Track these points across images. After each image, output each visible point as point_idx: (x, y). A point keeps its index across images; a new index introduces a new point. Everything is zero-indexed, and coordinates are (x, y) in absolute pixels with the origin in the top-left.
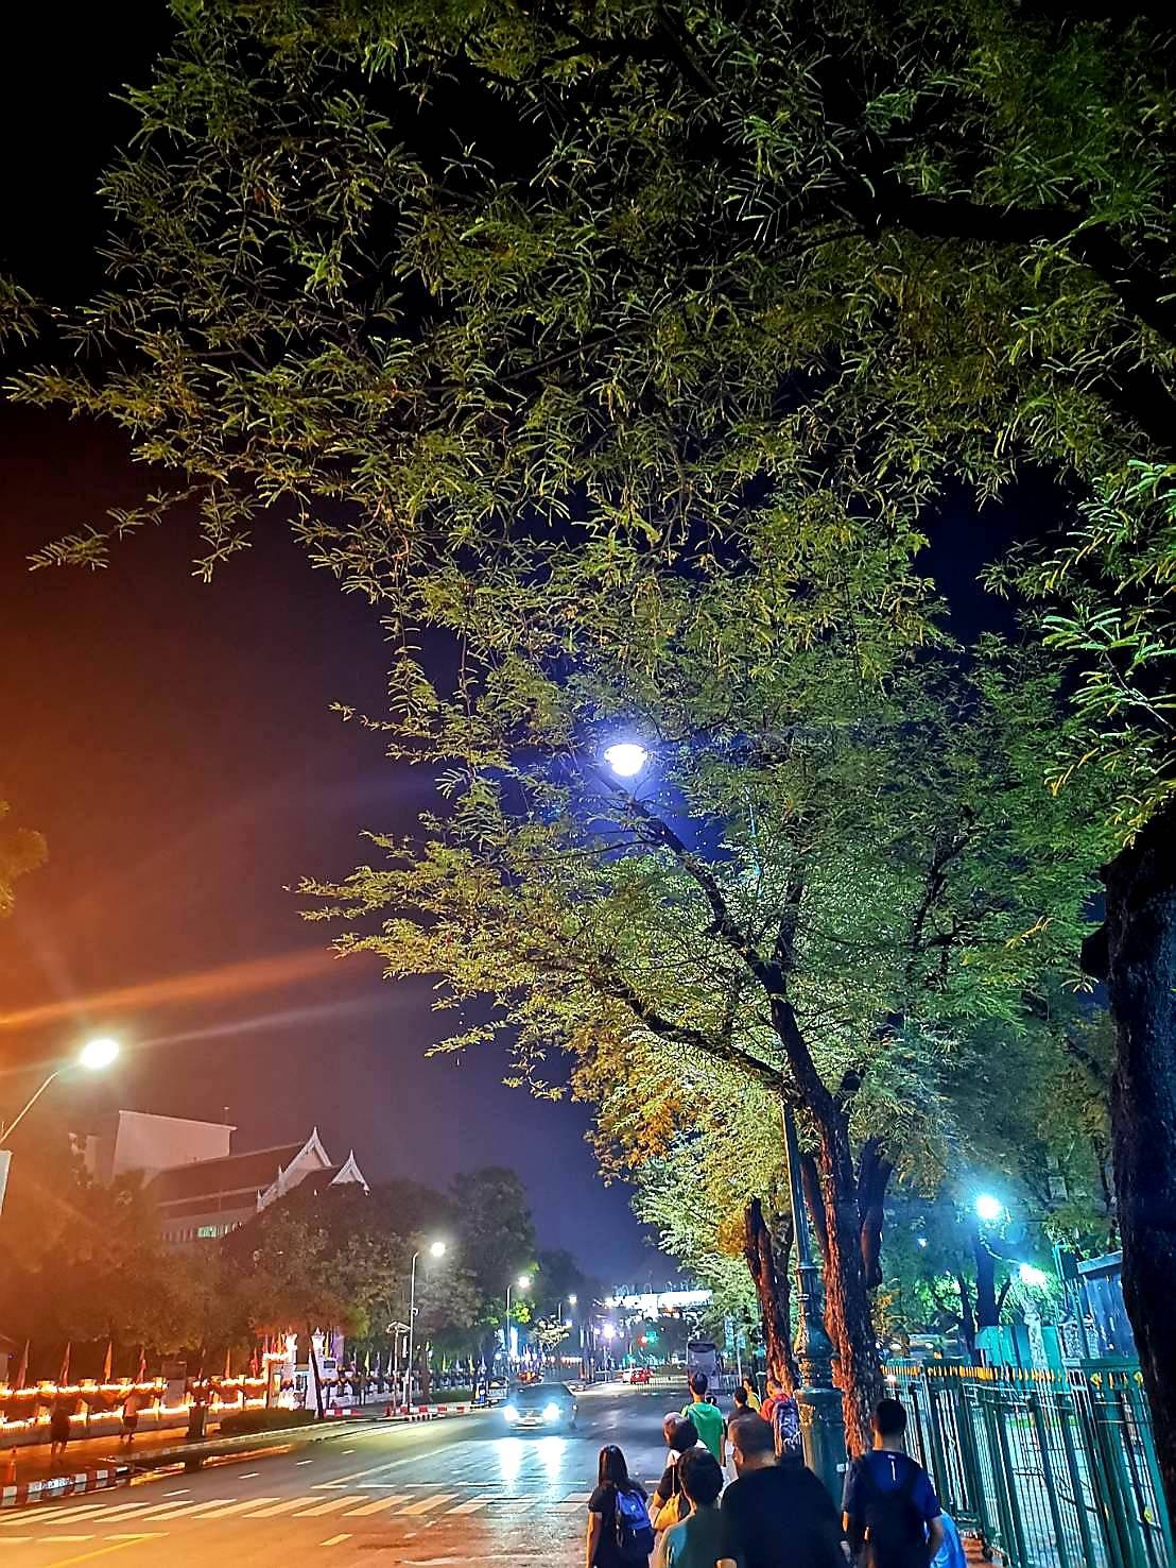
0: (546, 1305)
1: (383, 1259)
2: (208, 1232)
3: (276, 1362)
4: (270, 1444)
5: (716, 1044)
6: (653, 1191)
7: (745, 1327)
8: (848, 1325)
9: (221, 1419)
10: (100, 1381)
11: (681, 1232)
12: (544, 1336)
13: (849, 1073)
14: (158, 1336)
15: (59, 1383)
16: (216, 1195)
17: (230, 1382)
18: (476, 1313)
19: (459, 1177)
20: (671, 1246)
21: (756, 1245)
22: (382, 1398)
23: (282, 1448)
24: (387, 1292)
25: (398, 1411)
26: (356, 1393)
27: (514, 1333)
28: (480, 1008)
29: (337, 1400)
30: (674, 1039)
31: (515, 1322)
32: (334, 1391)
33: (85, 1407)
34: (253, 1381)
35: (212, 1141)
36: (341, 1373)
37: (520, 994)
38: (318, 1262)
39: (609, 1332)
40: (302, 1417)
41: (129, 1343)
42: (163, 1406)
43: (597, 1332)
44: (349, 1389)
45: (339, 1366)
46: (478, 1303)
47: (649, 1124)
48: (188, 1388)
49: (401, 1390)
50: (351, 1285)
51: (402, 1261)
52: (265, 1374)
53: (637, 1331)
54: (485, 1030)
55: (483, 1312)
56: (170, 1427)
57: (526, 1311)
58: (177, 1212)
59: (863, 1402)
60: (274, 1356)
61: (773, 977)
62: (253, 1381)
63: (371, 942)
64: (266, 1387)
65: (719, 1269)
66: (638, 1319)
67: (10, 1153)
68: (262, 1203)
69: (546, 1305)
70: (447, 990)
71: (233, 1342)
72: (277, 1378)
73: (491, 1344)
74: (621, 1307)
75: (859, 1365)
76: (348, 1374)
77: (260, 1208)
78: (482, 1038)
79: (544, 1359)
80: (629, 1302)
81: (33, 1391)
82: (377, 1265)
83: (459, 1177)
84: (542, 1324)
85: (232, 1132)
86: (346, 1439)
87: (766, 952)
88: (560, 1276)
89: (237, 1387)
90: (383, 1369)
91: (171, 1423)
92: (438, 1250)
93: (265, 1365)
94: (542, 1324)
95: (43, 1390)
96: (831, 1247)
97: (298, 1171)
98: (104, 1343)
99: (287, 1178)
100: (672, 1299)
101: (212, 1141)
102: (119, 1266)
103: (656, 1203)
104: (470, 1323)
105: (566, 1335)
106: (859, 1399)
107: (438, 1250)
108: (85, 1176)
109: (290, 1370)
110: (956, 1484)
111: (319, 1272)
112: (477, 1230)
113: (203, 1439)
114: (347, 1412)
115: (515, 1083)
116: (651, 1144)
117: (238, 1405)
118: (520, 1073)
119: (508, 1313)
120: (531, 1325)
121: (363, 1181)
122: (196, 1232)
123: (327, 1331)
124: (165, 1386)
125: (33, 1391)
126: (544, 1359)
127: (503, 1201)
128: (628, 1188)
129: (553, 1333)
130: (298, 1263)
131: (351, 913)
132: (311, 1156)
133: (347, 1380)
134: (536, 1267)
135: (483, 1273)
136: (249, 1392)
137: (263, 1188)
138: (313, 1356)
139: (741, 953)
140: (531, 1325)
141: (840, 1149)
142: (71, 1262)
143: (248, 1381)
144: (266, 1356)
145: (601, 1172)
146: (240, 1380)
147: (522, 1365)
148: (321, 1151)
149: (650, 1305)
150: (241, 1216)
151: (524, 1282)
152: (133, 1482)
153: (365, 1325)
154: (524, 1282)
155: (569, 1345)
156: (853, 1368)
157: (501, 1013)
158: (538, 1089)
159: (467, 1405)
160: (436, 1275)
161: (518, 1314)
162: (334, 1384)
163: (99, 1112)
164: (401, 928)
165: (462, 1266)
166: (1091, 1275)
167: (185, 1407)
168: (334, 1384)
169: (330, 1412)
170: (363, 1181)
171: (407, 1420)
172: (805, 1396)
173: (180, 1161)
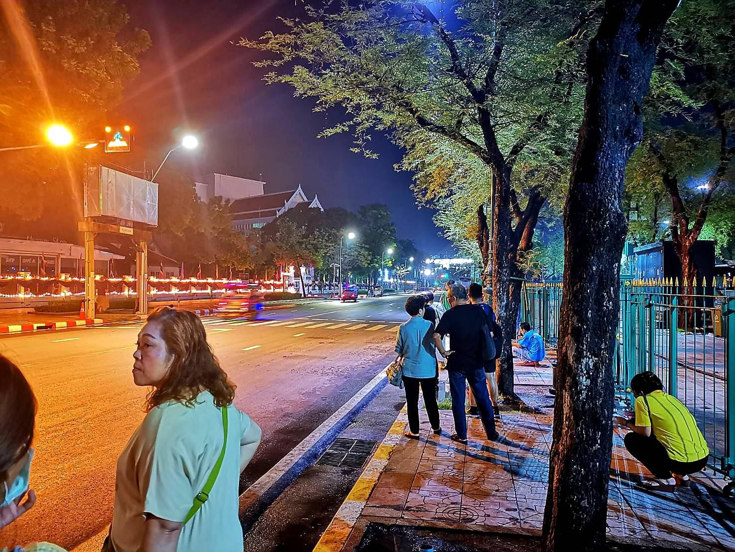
0: (399, 260)
1: (329, 239)
4: (283, 304)
5: (453, 133)
7: (479, 269)
8: (497, 258)
11: (455, 231)
12: (399, 272)
13: (515, 147)
14: (236, 263)
16: (258, 211)
17: (268, 282)
18: (369, 262)
19: (362, 207)
20: (449, 236)
21: (482, 234)
22: (330, 291)
24: (331, 252)
26: (320, 289)
27: (387, 272)
28: (338, 112)
29: (312, 291)
30: (431, 130)
31: (386, 267)
32: (311, 288)
34: (277, 283)
35: (255, 188)
36: (314, 282)
38: (303, 238)
39: (427, 272)
40: (297, 296)
43: (422, 272)
44: (317, 288)
45: (313, 279)
46: (370, 258)
50: (316, 249)
51: (336, 239)
52: (282, 280)
53: (439, 273)
54: (344, 126)
55: (372, 262)
57: (390, 262)
59: (499, 288)
61: (479, 96)
62: (277, 283)
64: (282, 285)
65: (469, 246)
66: (441, 268)
68: (278, 214)
69: (399, 260)
71: (267, 266)
72: (287, 282)
73: (376, 275)
74: (433, 263)
75: (500, 274)
76: (316, 282)
79: (399, 281)
80: (437, 262)
82: (326, 241)
83: (362, 207)
84: (398, 268)
86: (314, 304)
87: (478, 84)
88: (406, 249)
92: (352, 236)
93: (282, 277)
94: (398, 268)
96: (494, 226)
99: (288, 205)
100: (455, 261)
101: (255, 188)
102: (216, 235)
104: (366, 265)
106: (498, 287)
107: (352, 236)
109: (291, 278)
111: (302, 243)
112: (370, 229)
114: (315, 296)
115: (356, 150)
117: (272, 291)
118: (358, 146)
119: (383, 263)
120: (393, 268)
122: (252, 225)
123: (307, 265)
125: (188, 281)
126: (399, 281)
127: (381, 218)
128: (430, 211)
129: (402, 272)
130: (294, 239)
131: (277, 63)
132: (298, 197)
135: (372, 244)
137: (279, 208)
139: (464, 83)
141: (505, 182)
142: (196, 233)
143: (275, 282)
144: (282, 274)
145: (416, 203)
146: (272, 282)
147: (390, 284)
148: (303, 194)
149: (446, 263)
150: (270, 219)
151: (390, 251)
153: (321, 264)
154: (390, 251)
155: (410, 276)
156: (497, 275)
157: (350, 117)
158: (367, 154)
159: (365, 296)
162: (311, 285)
164: (299, 70)
165: (363, 243)
166: (639, 253)
168: (311, 285)
169: (310, 295)
171: (339, 299)
172: (487, 290)
173: (242, 197)
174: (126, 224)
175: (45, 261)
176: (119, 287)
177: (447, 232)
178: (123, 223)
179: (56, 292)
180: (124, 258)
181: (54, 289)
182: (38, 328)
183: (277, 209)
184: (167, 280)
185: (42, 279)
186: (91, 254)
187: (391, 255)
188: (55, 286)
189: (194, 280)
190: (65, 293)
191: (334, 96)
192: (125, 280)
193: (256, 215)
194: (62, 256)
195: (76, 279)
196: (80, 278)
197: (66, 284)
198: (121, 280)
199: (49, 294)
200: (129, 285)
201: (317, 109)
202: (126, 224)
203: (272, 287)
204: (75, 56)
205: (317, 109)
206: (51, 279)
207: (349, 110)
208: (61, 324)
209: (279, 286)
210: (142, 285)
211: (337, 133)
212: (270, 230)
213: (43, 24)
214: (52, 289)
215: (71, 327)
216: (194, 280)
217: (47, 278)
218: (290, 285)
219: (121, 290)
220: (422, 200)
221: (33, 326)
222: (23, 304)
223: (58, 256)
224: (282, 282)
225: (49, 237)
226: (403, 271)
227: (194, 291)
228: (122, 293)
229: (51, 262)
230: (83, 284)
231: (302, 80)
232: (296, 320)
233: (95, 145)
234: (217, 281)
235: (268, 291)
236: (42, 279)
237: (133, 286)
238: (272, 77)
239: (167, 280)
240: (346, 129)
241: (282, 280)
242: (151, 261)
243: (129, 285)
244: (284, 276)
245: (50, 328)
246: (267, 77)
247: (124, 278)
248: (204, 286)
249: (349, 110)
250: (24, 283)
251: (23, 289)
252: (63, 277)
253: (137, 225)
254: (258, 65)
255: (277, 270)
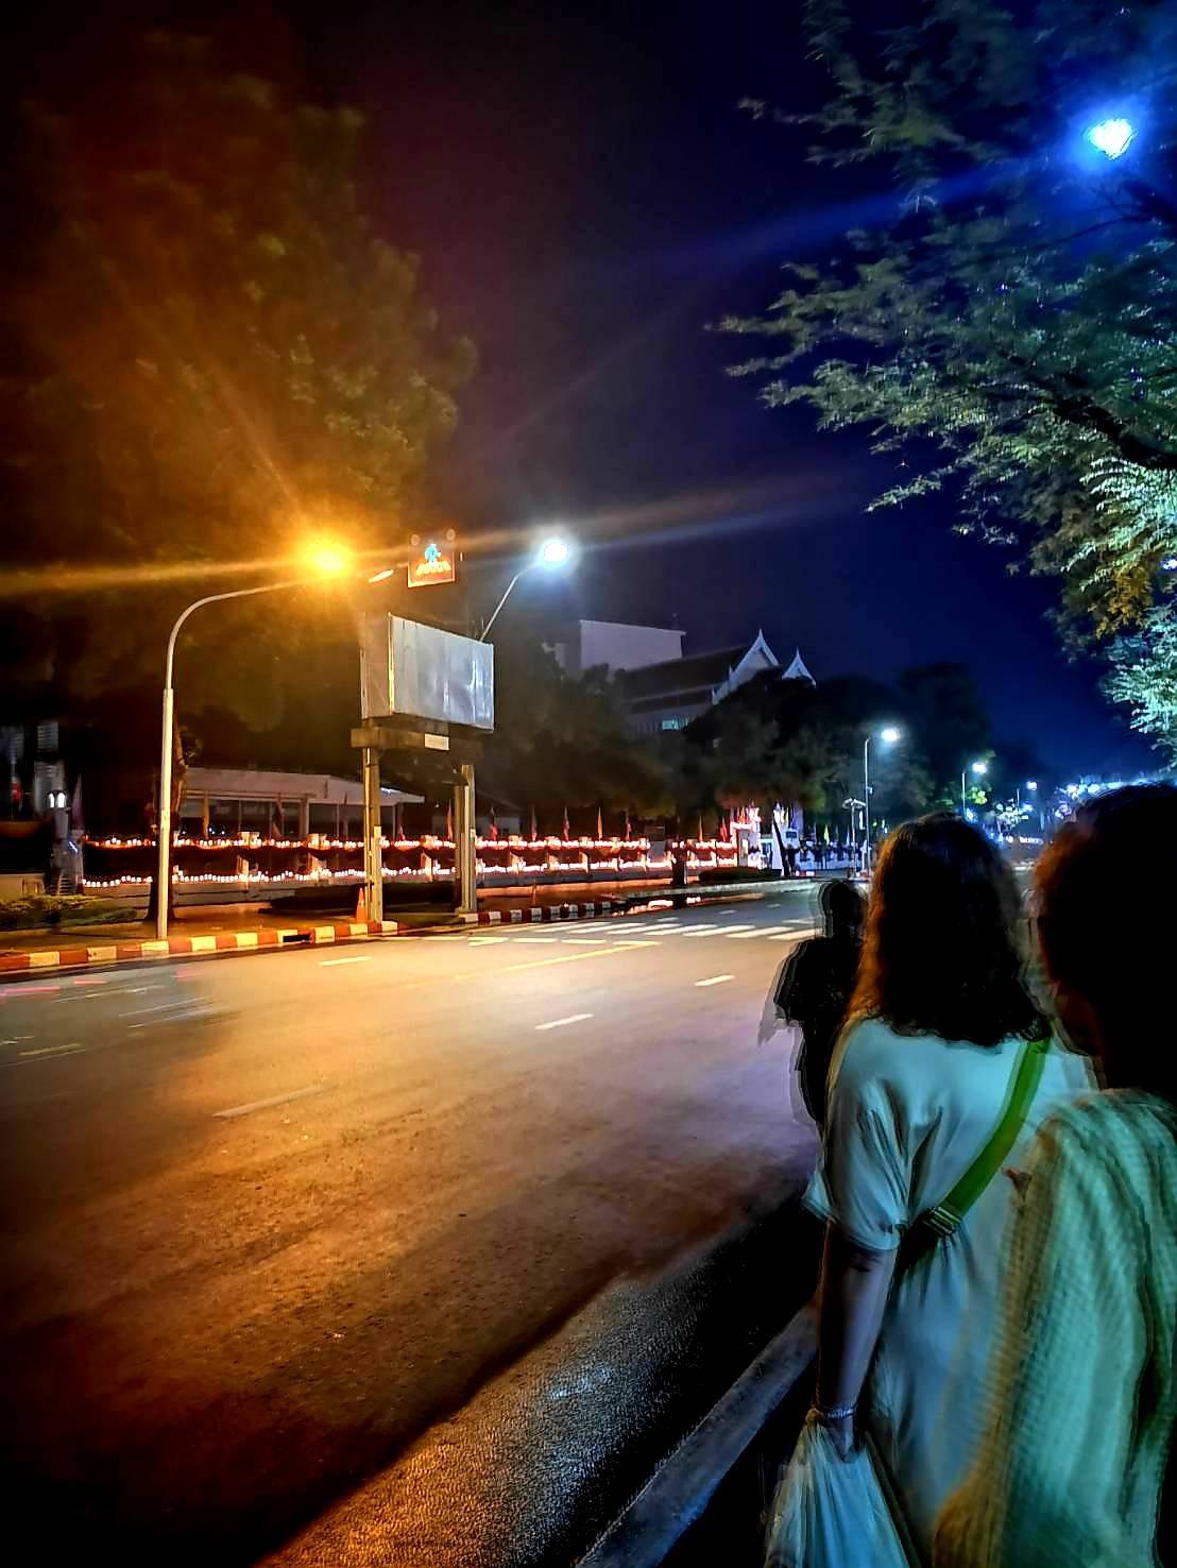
2: (671, 724)
3: (743, 830)
4: (749, 892)
6: (1123, 670)
9: (699, 872)
10: (595, 838)
12: (1002, 817)
15: (562, 839)
17: (704, 845)
18: (931, 794)
20: (1145, 724)
23: (754, 896)
25: (858, 874)
26: (818, 859)
28: (922, 449)
33: (585, 858)
35: (663, 645)
36: (803, 843)
37: (969, 435)
40: (769, 874)
41: (616, 810)
42: (649, 860)
44: (810, 855)
47: (1122, 590)
48: (668, 848)
49: (860, 858)
50: (805, 770)
51: (852, 748)
52: (733, 839)
54: (932, 479)
55: (937, 794)
56: (657, 877)
57: (982, 794)
58: (637, 708)
60: (741, 826)
63: (801, 391)
64: (736, 851)
67: (492, 645)
68: (716, 698)
70: (889, 432)
71: (701, 812)
72: (745, 843)
76: (809, 844)
77: (715, 702)
78: (927, 487)
81: (542, 844)
85: (682, 637)
89: (710, 849)
90: (842, 840)
91: (656, 874)
92: (890, 736)
93: (733, 832)
94: (1000, 807)
95: (549, 844)
97: (746, 669)
98: (594, 810)
99: (737, 676)
101: (663, 645)
103: (1128, 682)
105: (1026, 817)
107: (890, 736)
108: (557, 670)
110: (822, 1284)
113: (685, 886)
114: (809, 874)
116: (1123, 610)
117: (712, 863)
120: (988, 807)
121: (810, 676)
122: (660, 725)
123: (787, 806)
124: (649, 846)
125: (542, 844)
128: (1097, 669)
130: (755, 750)
131: (779, 362)
132: (757, 657)
133: (809, 848)
134: (992, 754)
136: (720, 853)
138: (776, 827)
140: (988, 807)
144: (733, 825)
146: (712, 844)
148: (767, 651)
150: (698, 710)
151: (980, 768)
152: (632, 911)
157: (948, 457)
158: (991, 535)
160: (888, 759)
161: (974, 796)
163: (557, 613)
164: (833, 373)
167: (667, 862)
170: (810, 676)
174: (436, 728)
175: (282, 811)
176: (414, 859)
177: (1140, 714)
178: (430, 727)
179: (303, 871)
180: (421, 800)
181: (298, 864)
182: (286, 939)
183: (712, 686)
184: (503, 844)
185: (279, 845)
186: (370, 794)
187: (985, 777)
188: (298, 859)
189: (554, 842)
190: (318, 873)
191: (910, 414)
192: (426, 845)
193: (671, 702)
194: (311, 800)
195: (336, 843)
196: (344, 842)
197: (322, 855)
198: (417, 844)
199: (291, 874)
200: (434, 854)
201: (881, 448)
202: (436, 728)
203: (713, 855)
204: (351, 407)
205: (881, 448)
206: (295, 845)
207: (947, 443)
208: (325, 932)
209: (729, 854)
210: (373, 856)
211: (913, 497)
212: (698, 733)
213: (292, 351)
214: (293, 866)
215: (342, 941)
216: (554, 842)
217: (288, 843)
218: (753, 850)
219: (417, 865)
220: (1075, 642)
221: (276, 935)
222: (245, 894)
223: (304, 800)
224: (733, 844)
225: (287, 765)
226: (1012, 814)
227: (555, 865)
228: (420, 872)
229: (292, 812)
230: (359, 853)
231: (840, 393)
232: (791, 925)
233: (390, 573)
234: (599, 844)
235: (704, 864)
236: (279, 845)
237: (445, 857)
238: (778, 394)
239: (503, 844)
240: (935, 485)
241: (733, 839)
242: (481, 808)
243: (434, 854)
244: (738, 831)
245: (304, 941)
246: (769, 393)
247: (424, 840)
248: (572, 856)
249: (947, 443)
250: (247, 853)
251: (246, 865)
252: (316, 841)
253: (456, 731)
254: (738, 371)
255: (725, 816)
